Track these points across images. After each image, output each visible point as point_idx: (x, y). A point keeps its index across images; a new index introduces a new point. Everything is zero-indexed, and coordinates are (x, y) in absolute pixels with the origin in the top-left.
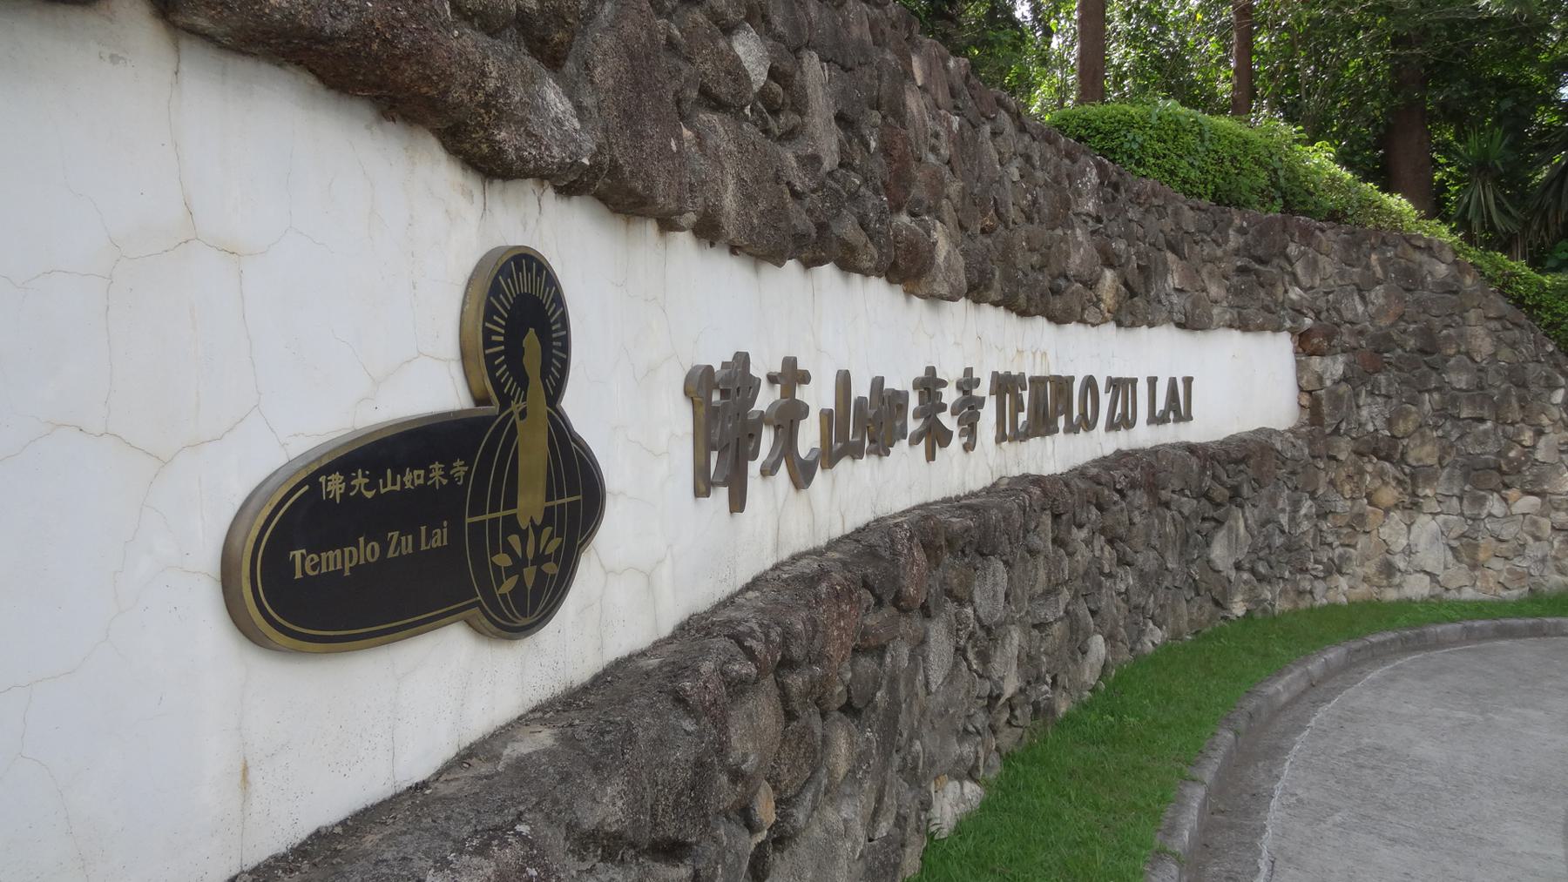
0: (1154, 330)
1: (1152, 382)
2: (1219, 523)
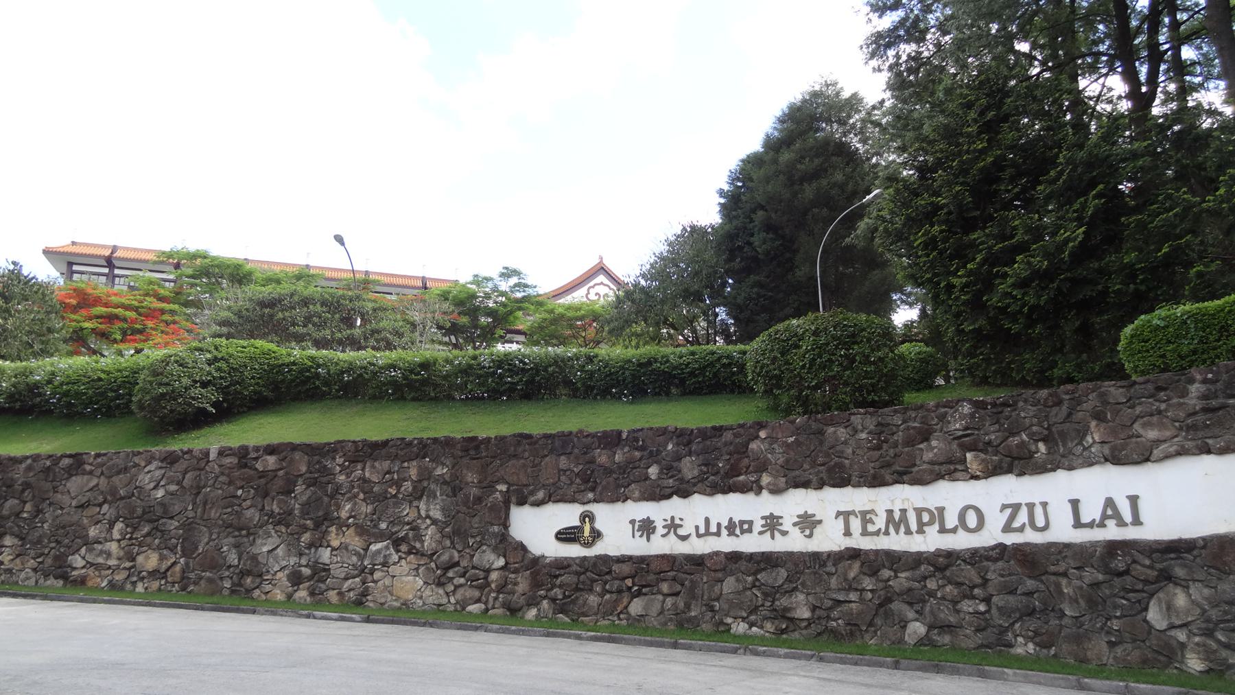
1: (1075, 504)
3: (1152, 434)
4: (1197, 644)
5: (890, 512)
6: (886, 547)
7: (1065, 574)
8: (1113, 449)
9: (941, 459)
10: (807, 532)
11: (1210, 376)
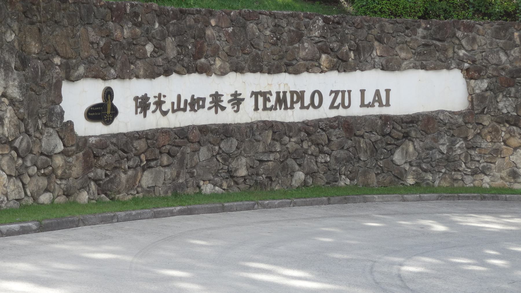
0: (363, 72)
1: (363, 92)
2: (398, 146)
3: (403, 55)
4: (414, 171)
5: (278, 93)
6: (279, 119)
7: (362, 136)
8: (387, 61)
9: (309, 58)
10: (236, 109)
11: (428, 26)
